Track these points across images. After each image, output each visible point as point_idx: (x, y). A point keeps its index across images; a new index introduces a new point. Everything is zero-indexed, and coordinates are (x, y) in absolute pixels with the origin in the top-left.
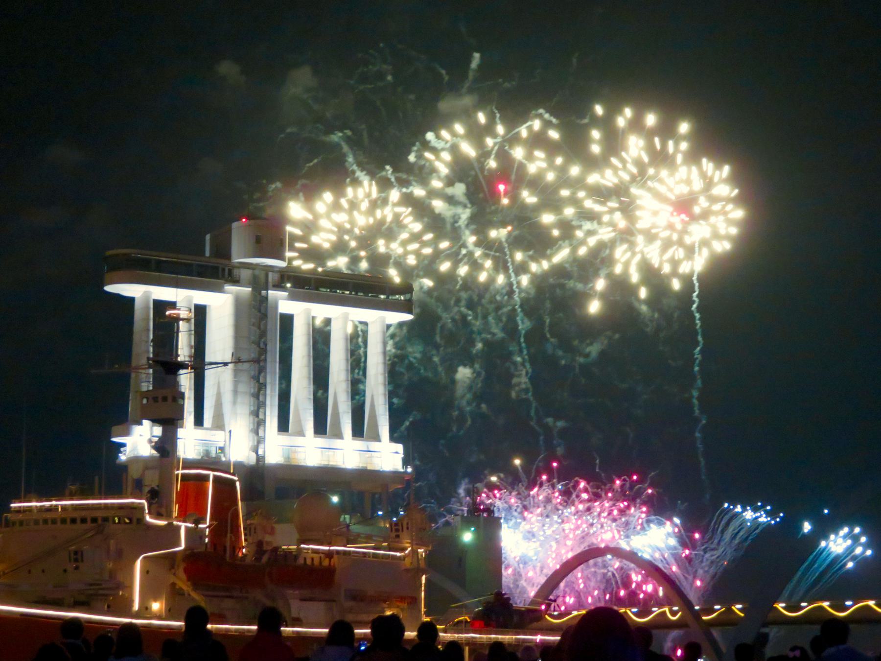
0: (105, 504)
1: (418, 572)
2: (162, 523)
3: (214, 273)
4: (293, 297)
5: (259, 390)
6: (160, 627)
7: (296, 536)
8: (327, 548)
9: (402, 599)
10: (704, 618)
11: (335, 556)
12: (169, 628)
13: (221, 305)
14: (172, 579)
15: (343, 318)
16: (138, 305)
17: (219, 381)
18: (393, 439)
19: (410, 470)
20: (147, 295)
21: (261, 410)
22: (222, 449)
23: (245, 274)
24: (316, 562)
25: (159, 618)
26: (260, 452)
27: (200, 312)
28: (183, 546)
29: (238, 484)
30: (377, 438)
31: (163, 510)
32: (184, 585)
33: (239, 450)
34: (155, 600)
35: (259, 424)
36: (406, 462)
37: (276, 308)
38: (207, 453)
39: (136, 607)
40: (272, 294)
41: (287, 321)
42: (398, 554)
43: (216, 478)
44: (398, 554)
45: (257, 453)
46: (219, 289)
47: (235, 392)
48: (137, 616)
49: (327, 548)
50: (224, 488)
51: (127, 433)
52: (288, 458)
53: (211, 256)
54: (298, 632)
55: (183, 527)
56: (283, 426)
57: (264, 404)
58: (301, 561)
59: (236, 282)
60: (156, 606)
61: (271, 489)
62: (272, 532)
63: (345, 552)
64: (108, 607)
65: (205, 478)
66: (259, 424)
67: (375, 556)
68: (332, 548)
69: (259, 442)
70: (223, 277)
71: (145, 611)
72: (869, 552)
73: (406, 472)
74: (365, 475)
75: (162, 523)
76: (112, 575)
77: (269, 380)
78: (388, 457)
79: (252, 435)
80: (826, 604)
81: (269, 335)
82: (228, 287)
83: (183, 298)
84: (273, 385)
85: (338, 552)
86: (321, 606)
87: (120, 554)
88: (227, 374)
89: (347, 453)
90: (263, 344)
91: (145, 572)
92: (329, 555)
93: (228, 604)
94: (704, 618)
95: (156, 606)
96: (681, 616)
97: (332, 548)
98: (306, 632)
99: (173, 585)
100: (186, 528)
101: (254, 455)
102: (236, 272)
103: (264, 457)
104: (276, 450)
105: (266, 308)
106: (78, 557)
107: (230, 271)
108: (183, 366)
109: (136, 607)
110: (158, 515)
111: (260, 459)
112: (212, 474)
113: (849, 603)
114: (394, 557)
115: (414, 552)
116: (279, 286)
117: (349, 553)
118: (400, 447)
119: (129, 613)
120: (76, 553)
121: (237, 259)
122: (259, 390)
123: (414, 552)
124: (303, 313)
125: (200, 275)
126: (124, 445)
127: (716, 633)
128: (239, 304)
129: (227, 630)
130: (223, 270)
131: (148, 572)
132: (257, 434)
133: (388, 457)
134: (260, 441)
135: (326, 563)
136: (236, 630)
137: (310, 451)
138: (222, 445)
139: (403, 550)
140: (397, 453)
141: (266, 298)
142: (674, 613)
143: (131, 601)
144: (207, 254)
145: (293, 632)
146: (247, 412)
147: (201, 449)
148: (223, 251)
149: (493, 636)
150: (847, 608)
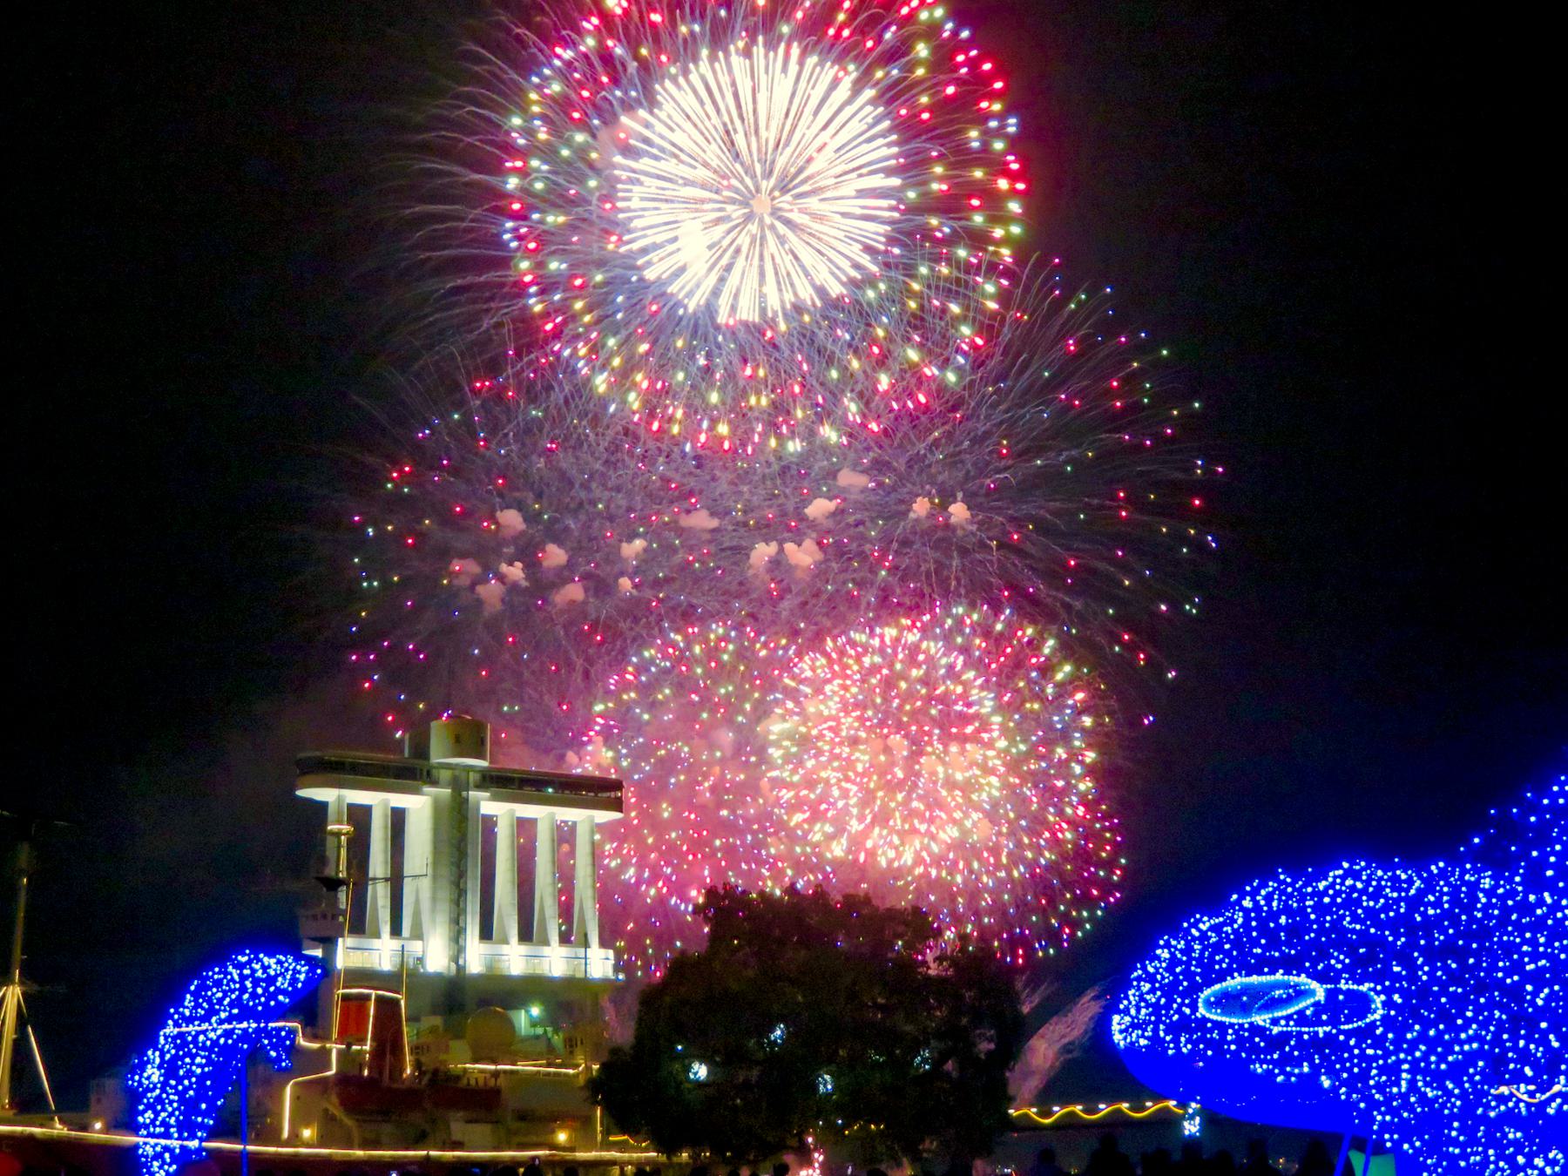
2: (315, 1046)
3: (411, 774)
4: (495, 798)
5: (460, 896)
7: (469, 1054)
8: (493, 1067)
9: (574, 1118)
12: (317, 1155)
13: (419, 806)
16: (331, 810)
17: (419, 889)
19: (621, 977)
22: (420, 960)
23: (445, 775)
24: (481, 1082)
26: (461, 962)
27: (398, 819)
28: (333, 1071)
29: (403, 1003)
31: (321, 1032)
32: (338, 1112)
33: (435, 957)
34: (307, 1126)
35: (458, 935)
37: (478, 809)
39: (285, 1134)
40: (473, 794)
43: (379, 999)
46: (416, 791)
47: (434, 899)
48: (287, 1144)
49: (493, 1067)
50: (388, 1008)
52: (490, 967)
55: (335, 1048)
56: (486, 934)
57: (465, 911)
58: (465, 1081)
59: (434, 783)
60: (307, 1133)
61: (467, 1003)
62: (447, 1049)
63: (512, 1072)
64: (257, 1135)
65: (367, 998)
66: (458, 935)
67: (549, 1074)
70: (421, 778)
71: (295, 1139)
73: (822, 1165)
75: (315, 1046)
77: (469, 885)
82: (427, 789)
83: (379, 801)
84: (474, 891)
85: (505, 1072)
88: (426, 884)
89: (555, 961)
90: (462, 840)
91: (296, 1099)
92: (496, 1074)
93: (387, 1129)
95: (307, 1133)
99: (326, 1110)
101: (453, 966)
102: (434, 772)
104: (476, 958)
107: (429, 773)
108: (341, 882)
109: (285, 1134)
110: (314, 1037)
111: (461, 969)
112: (373, 993)
114: (566, 1075)
116: (480, 786)
117: (517, 1072)
119: (272, 1136)
121: (437, 757)
122: (460, 896)
123: (588, 1068)
125: (397, 777)
128: (437, 807)
134: (458, 949)
135: (492, 1083)
137: (515, 959)
138: (420, 955)
141: (467, 800)
143: (280, 1130)
148: (421, 751)
150: (1145, 1109)
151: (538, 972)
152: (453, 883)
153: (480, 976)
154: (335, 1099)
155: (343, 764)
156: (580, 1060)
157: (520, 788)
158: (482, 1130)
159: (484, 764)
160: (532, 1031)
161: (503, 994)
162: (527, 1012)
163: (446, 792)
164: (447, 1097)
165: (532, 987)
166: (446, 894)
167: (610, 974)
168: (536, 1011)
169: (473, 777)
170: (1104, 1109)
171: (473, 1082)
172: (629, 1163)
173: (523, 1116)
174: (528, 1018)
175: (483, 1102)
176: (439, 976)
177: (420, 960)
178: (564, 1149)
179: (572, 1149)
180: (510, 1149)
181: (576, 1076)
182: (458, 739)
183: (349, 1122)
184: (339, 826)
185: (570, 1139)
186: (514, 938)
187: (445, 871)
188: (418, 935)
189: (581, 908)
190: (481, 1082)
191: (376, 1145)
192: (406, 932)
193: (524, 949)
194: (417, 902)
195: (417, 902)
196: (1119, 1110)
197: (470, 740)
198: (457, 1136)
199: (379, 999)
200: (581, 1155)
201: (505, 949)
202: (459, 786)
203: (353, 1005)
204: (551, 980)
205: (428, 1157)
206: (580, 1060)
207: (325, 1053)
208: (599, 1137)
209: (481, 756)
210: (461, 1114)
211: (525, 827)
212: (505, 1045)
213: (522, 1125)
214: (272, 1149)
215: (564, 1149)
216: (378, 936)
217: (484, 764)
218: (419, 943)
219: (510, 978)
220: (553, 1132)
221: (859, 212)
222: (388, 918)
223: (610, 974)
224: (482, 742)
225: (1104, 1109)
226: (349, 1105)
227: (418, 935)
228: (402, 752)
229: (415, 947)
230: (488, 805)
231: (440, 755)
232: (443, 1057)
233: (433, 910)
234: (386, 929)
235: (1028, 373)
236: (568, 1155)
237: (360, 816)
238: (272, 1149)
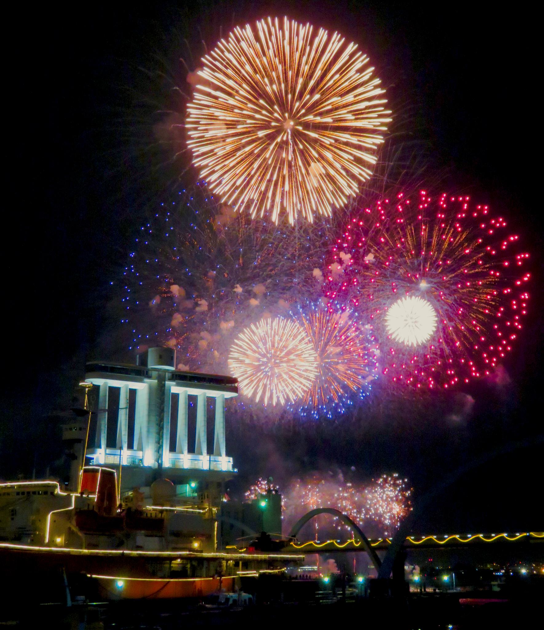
0: (35, 484)
1: (212, 521)
2: (65, 494)
3: (140, 373)
4: (178, 385)
6: (57, 552)
8: (160, 508)
9: (203, 535)
10: (372, 545)
11: (165, 513)
12: (62, 552)
13: (142, 388)
14: (69, 525)
15: (201, 394)
18: (228, 454)
20: (106, 384)
21: (161, 441)
23: (154, 374)
24: (153, 515)
25: (61, 547)
26: (160, 462)
27: (133, 393)
28: (73, 507)
30: (220, 455)
32: (75, 529)
33: (148, 459)
34: (59, 536)
36: (234, 466)
37: (170, 390)
38: (134, 462)
39: (47, 540)
40: (168, 383)
41: (175, 397)
42: (201, 511)
43: (102, 470)
44: (201, 511)
45: (158, 462)
46: (141, 381)
47: (148, 431)
48: (48, 545)
49: (160, 508)
51: (93, 453)
52: (174, 464)
53: (139, 365)
54: (140, 554)
56: (173, 449)
57: (162, 436)
58: (145, 515)
59: (150, 377)
60: (59, 540)
61: (163, 480)
64: (32, 540)
65: (97, 471)
68: (164, 508)
69: (159, 457)
70: (143, 375)
71: (52, 543)
72: (236, 470)
73: (234, 472)
74: (212, 473)
76: (34, 522)
78: (225, 464)
79: (156, 453)
80: (481, 536)
81: (166, 403)
82: (146, 380)
85: (167, 510)
86: (156, 539)
87: (38, 511)
89: (204, 462)
90: (162, 403)
91: (53, 522)
92: (162, 511)
94: (372, 545)
96: (360, 545)
97: (164, 508)
98: (145, 554)
99: (70, 528)
100: (94, 498)
101: (157, 464)
102: (150, 372)
103: (162, 464)
105: (164, 389)
106: (14, 513)
107: (147, 372)
109: (47, 540)
111: (160, 465)
112: (100, 468)
113: (493, 535)
114: (199, 513)
115: (210, 510)
118: (231, 459)
119: (42, 544)
120: (12, 511)
121: (151, 366)
123: (210, 510)
124: (182, 391)
126: (93, 459)
127: (378, 553)
128: (150, 388)
129: (97, 553)
130: (144, 371)
131: (55, 521)
132: (159, 452)
133: (225, 464)
134: (159, 457)
136: (103, 553)
137: (186, 461)
138: (141, 458)
139: (204, 509)
140: (229, 462)
141: (164, 385)
142: (357, 543)
143: (43, 537)
144: (137, 364)
145: (137, 554)
146: (154, 441)
147: (130, 460)
148: (144, 362)
149: (255, 555)
150: (468, 538)
151: (197, 467)
152: (157, 424)
153: (169, 469)
154: (74, 522)
155: (107, 367)
156: (206, 505)
157: (190, 380)
158: (155, 541)
159: (172, 369)
160: (191, 495)
161: (180, 477)
162: (190, 485)
163: (155, 382)
164: (136, 522)
165: (194, 474)
166: (154, 429)
167: (231, 469)
168: (193, 485)
169: (168, 375)
170: (471, 537)
171: (149, 515)
172: (230, 559)
173: (177, 534)
174: (189, 488)
175: (155, 526)
176: (150, 468)
177: (141, 460)
178: (197, 551)
179: (201, 552)
180: (167, 551)
181: (204, 514)
182: (161, 357)
183: (80, 534)
184: (104, 394)
185: (200, 546)
186: (186, 451)
187: (154, 418)
188: (141, 449)
189: (218, 438)
190: (153, 515)
191: (95, 546)
192: (135, 447)
193: (190, 456)
194: (141, 433)
195: (141, 433)
196: (478, 538)
197: (166, 357)
198: (139, 543)
199: (102, 470)
200: (206, 555)
201: (181, 456)
202: (161, 379)
203: (90, 474)
204: (202, 471)
205: (123, 554)
206: (206, 505)
207: (69, 497)
208: (216, 545)
209: (171, 365)
210: (143, 532)
211: (192, 400)
212: (173, 499)
213: (175, 538)
214: (37, 548)
215: (197, 551)
216: (121, 448)
217: (172, 369)
218: (141, 452)
219: (183, 470)
220: (191, 542)
221: (347, 158)
222: (126, 440)
223: (231, 469)
224: (172, 358)
225: (471, 537)
226: (81, 526)
227: (141, 449)
228: (136, 362)
229: (140, 454)
230: (174, 388)
231: (152, 364)
232: (140, 503)
233: (148, 436)
234: (125, 446)
235: (304, 527)
236: (199, 555)
237: (114, 393)
238: (37, 548)
